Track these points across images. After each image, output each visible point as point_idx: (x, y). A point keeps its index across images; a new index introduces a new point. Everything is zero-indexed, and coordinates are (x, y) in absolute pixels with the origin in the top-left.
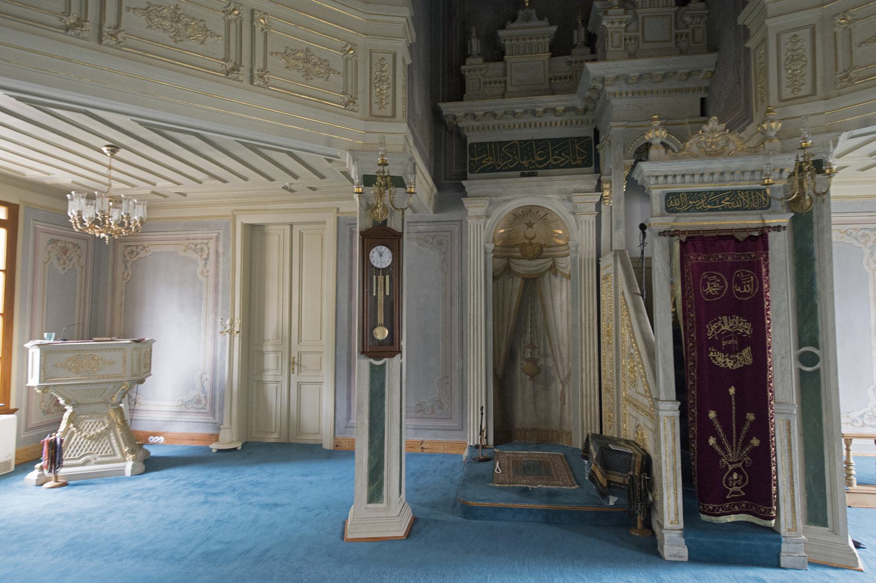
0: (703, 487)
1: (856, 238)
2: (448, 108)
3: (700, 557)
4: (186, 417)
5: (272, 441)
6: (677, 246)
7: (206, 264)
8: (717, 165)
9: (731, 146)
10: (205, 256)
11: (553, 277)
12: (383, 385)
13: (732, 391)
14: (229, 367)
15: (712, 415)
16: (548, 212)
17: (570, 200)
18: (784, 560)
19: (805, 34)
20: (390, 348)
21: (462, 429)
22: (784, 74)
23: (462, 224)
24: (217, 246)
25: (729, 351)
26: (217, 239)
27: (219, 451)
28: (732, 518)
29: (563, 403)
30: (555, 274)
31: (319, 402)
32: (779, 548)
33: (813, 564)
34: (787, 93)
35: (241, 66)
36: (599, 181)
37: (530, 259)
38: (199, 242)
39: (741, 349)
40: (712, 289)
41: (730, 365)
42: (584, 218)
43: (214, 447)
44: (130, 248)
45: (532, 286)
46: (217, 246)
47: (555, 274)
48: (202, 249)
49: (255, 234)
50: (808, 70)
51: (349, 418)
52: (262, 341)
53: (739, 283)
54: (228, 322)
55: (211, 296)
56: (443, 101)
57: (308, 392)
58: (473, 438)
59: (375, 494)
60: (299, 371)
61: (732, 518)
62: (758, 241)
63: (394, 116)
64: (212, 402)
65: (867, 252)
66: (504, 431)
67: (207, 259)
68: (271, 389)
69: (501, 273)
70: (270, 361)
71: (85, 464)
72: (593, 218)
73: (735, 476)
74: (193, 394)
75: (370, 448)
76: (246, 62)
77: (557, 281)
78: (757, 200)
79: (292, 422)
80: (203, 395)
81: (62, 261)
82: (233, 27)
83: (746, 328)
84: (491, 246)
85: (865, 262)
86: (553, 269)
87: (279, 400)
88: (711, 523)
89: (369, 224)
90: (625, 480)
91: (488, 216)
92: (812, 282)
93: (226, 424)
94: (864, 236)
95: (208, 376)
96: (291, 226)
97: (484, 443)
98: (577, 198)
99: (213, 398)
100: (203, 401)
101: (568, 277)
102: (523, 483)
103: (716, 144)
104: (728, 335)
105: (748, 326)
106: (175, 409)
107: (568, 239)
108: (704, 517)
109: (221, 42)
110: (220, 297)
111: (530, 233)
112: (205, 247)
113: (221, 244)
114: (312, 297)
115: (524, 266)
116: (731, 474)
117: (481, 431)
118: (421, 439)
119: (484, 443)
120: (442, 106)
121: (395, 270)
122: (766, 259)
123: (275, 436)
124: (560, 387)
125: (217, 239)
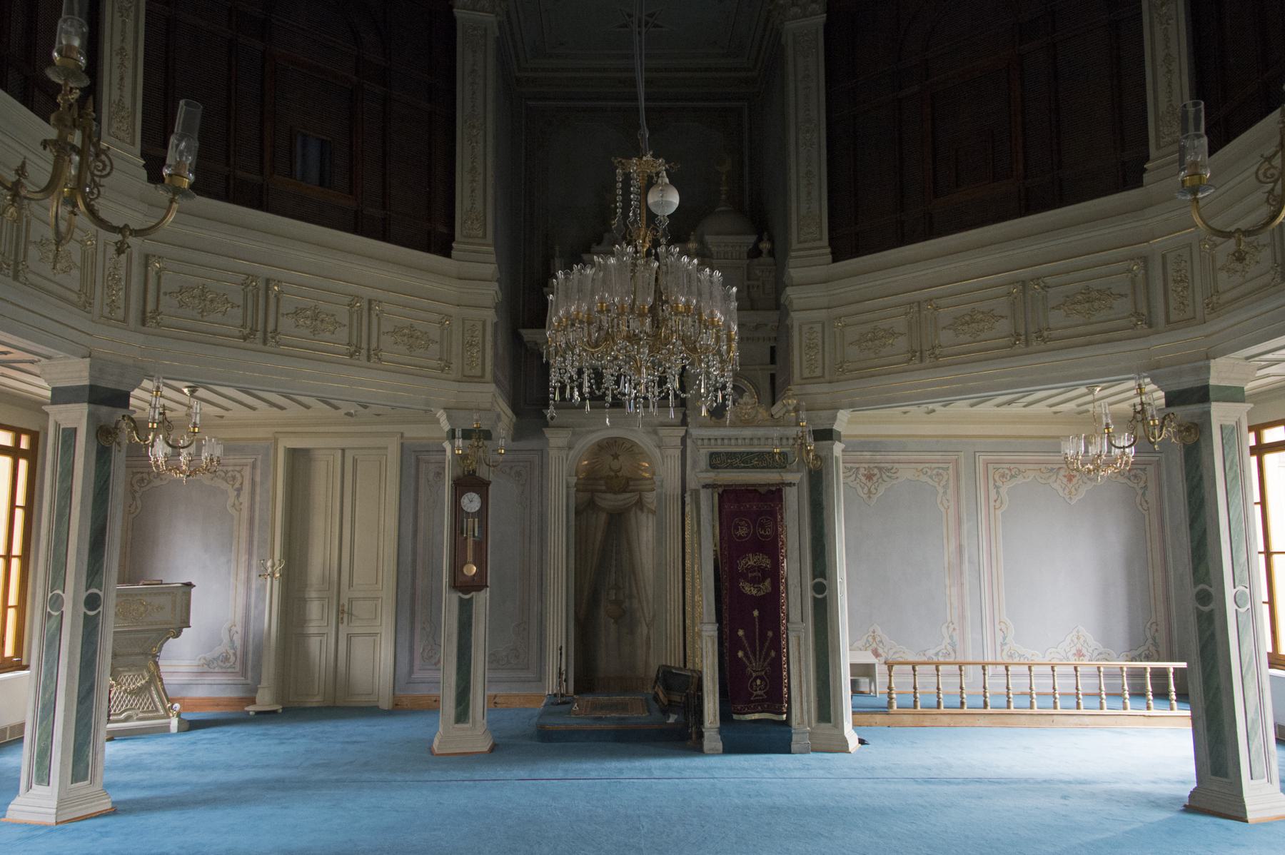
0: (732, 696)
1: (931, 477)
2: (528, 334)
3: (731, 748)
4: (209, 679)
5: (314, 705)
6: (716, 496)
7: (238, 496)
8: (748, 432)
9: (760, 417)
10: (237, 485)
11: (639, 513)
12: (470, 617)
13: (756, 613)
14: (268, 618)
15: (741, 633)
16: (634, 444)
17: (656, 433)
18: (794, 747)
19: (818, 327)
20: (477, 584)
21: (540, 680)
22: (804, 358)
23: (542, 453)
24: (253, 475)
25: (753, 581)
26: (254, 467)
27: (258, 713)
28: (756, 716)
29: (649, 648)
30: (642, 510)
31: (375, 657)
32: (791, 739)
33: (814, 751)
34: (806, 374)
35: (362, 351)
36: (685, 415)
37: (615, 493)
38: (230, 468)
39: (764, 580)
40: (742, 532)
41: (754, 592)
42: (670, 452)
43: (251, 709)
44: (139, 476)
45: (618, 523)
46: (253, 475)
47: (642, 510)
48: (234, 478)
49: (299, 459)
50: (819, 356)
51: (411, 672)
52: (304, 586)
53: (762, 526)
54: (269, 564)
55: (244, 534)
56: (524, 327)
57: (361, 649)
58: (551, 685)
59: (462, 714)
60: (350, 621)
61: (756, 716)
62: (774, 495)
63: (483, 376)
64: (245, 660)
65: (941, 490)
66: (586, 678)
67: (239, 490)
68: (314, 644)
69: (584, 508)
70: (314, 609)
71: (126, 720)
72: (678, 453)
73: (758, 682)
74: (219, 650)
75: (458, 674)
76: (364, 345)
77: (643, 517)
78: (782, 462)
79: (340, 680)
80: (231, 652)
81: (1082, 639)
82: (355, 316)
83: (766, 562)
84: (574, 480)
85: (939, 500)
86: (640, 504)
87: (324, 656)
88: (740, 721)
89: (459, 472)
90: (679, 689)
91: (570, 448)
92: (822, 527)
93: (264, 683)
94: (938, 474)
95: (239, 628)
96: (343, 450)
97: (563, 691)
98: (664, 432)
99: (245, 653)
100: (232, 659)
101: (654, 513)
102: (598, 714)
103: (749, 414)
104: (752, 569)
105: (768, 561)
106: (195, 669)
107: (654, 474)
108: (735, 717)
109: (346, 329)
110: (256, 534)
111: (615, 464)
112: (238, 475)
113: (258, 472)
114: (363, 534)
115: (609, 501)
116: (755, 680)
117: (560, 674)
118: (494, 693)
119: (563, 691)
120: (523, 332)
121: (483, 513)
122: (781, 508)
123: (318, 698)
124: (645, 628)
125: (254, 467)
